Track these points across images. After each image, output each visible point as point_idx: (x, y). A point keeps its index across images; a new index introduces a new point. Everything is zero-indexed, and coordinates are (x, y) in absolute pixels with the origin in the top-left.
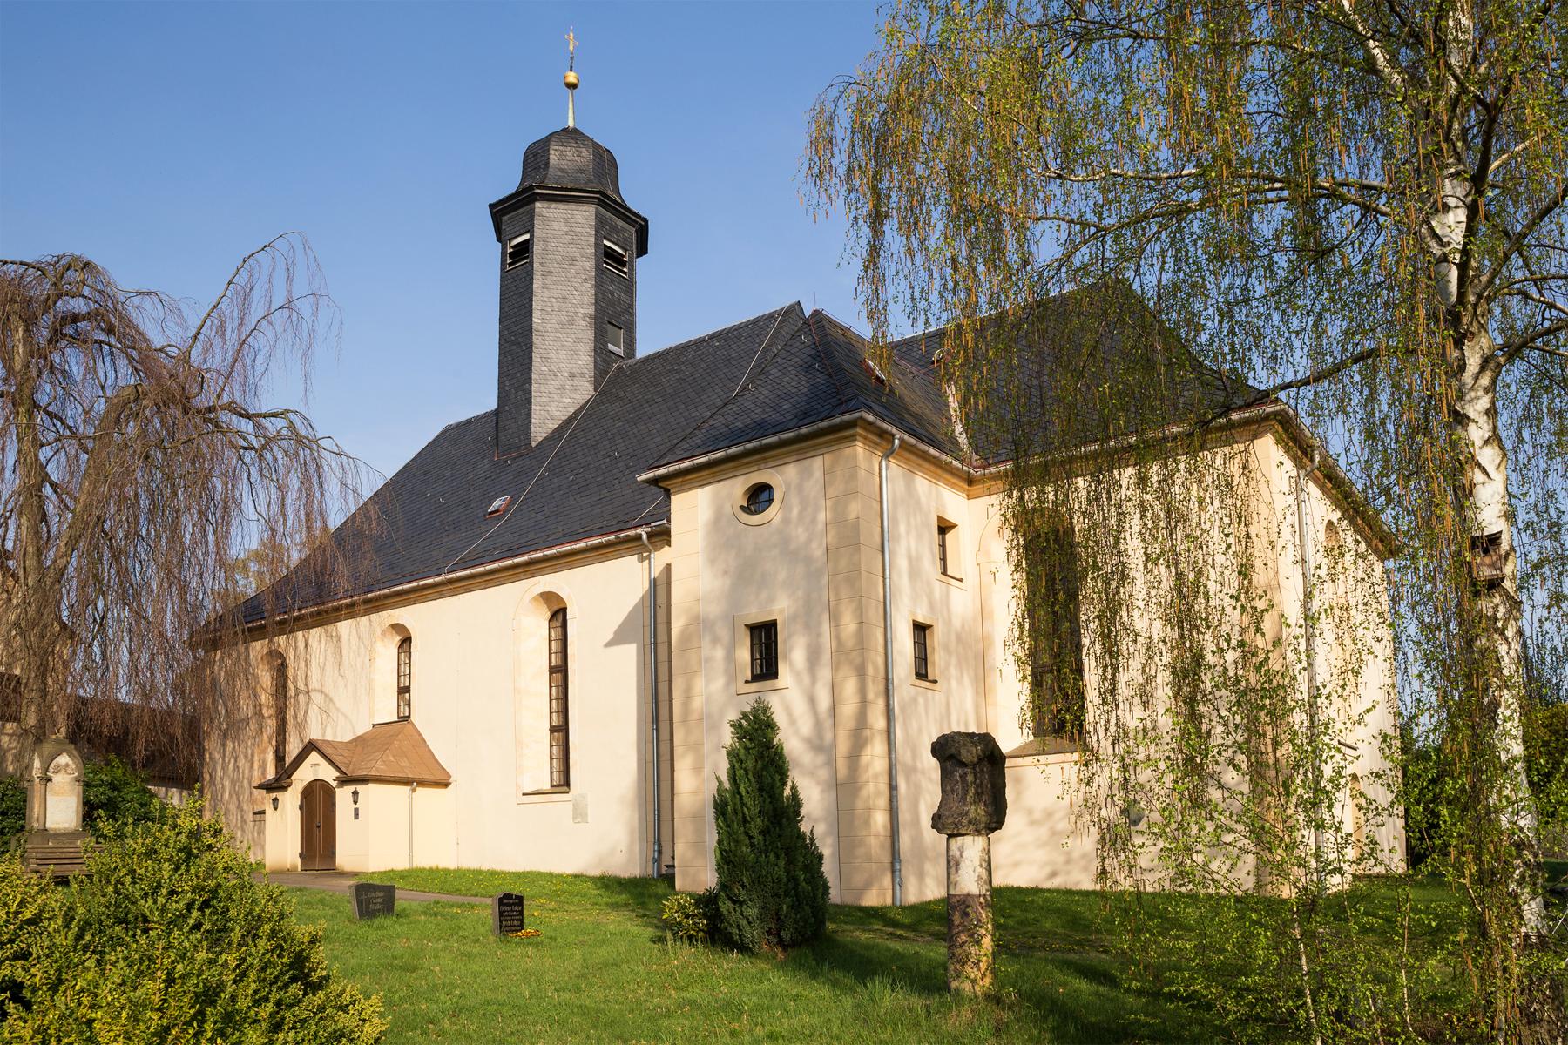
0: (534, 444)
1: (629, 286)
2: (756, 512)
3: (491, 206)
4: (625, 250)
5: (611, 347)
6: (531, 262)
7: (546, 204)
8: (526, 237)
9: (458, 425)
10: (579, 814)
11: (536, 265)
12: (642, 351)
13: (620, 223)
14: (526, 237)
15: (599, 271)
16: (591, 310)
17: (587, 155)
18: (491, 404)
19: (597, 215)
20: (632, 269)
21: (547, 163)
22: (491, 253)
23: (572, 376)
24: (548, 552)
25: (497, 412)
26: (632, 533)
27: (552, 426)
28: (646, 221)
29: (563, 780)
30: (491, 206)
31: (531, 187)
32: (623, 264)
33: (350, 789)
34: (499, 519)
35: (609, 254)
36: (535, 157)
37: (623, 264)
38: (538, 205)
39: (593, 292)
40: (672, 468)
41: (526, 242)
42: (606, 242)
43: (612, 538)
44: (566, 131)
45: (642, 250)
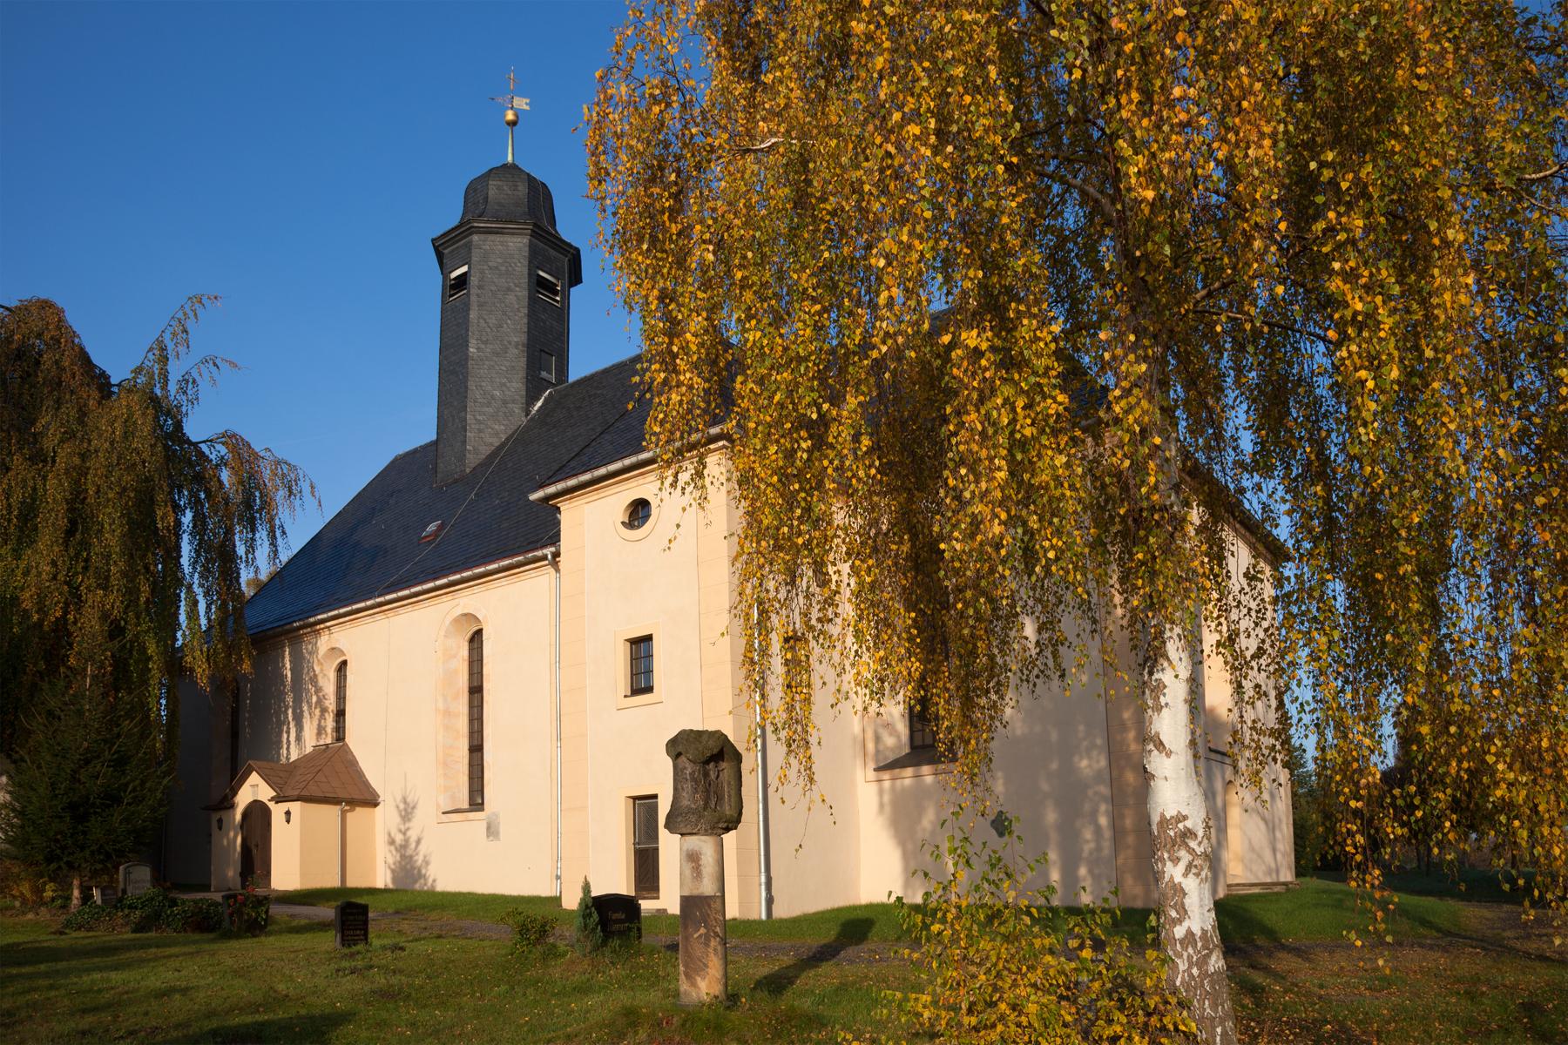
0: (468, 470)
1: (562, 315)
2: (639, 527)
3: (433, 241)
4: (558, 279)
5: (544, 374)
6: (468, 295)
7: (483, 237)
8: (464, 269)
9: (407, 454)
10: (492, 831)
11: (473, 298)
12: (576, 372)
13: (552, 252)
14: (464, 269)
15: (533, 301)
16: (523, 338)
17: (523, 189)
18: (434, 437)
19: (531, 245)
20: (566, 298)
21: (486, 198)
22: (432, 282)
23: (505, 402)
24: (465, 574)
25: (435, 444)
26: (539, 553)
27: (485, 451)
28: (578, 250)
29: (476, 800)
30: (433, 241)
31: (469, 222)
32: (556, 293)
33: (285, 806)
34: (430, 543)
35: (542, 283)
36: (475, 193)
37: (556, 293)
38: (475, 238)
39: (525, 320)
40: (560, 486)
41: (465, 274)
42: (542, 273)
43: (521, 558)
44: (505, 166)
45: (576, 278)
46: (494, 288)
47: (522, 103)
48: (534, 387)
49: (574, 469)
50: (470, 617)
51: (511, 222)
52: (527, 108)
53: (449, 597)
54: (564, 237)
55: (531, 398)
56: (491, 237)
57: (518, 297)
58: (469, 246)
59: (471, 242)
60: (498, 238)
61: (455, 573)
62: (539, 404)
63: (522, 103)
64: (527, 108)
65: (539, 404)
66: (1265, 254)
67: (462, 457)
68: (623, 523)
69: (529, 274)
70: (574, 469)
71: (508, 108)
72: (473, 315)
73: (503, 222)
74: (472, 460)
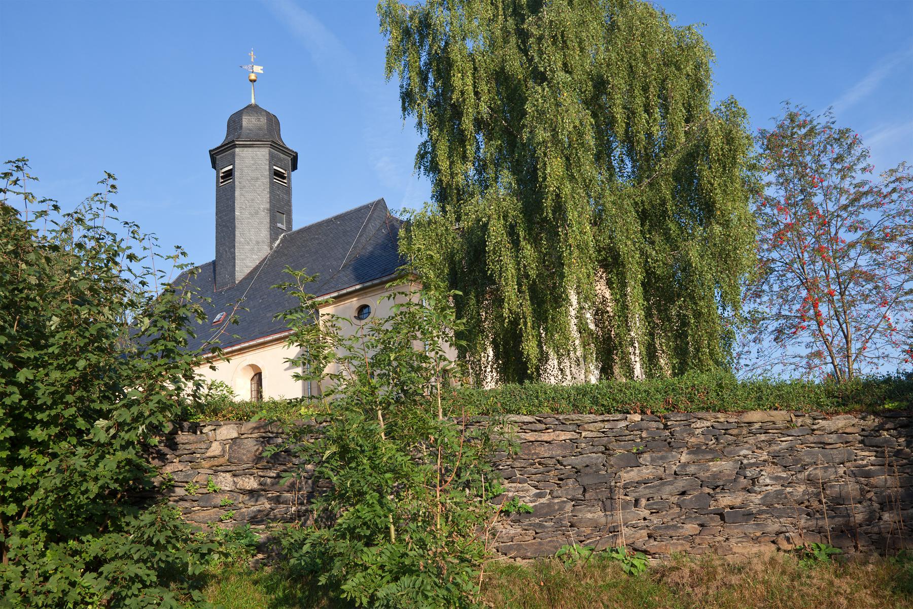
0: (237, 282)
1: (288, 191)
3: (210, 151)
5: (279, 225)
7: (241, 149)
8: (231, 167)
11: (237, 183)
13: (282, 156)
15: (272, 184)
16: (268, 206)
17: (263, 120)
19: (271, 155)
27: (247, 271)
28: (297, 154)
30: (210, 151)
31: (233, 141)
32: (284, 178)
36: (234, 123)
38: (237, 150)
42: (275, 167)
46: (249, 178)
47: (258, 69)
48: (274, 232)
49: (327, 290)
50: (253, 367)
51: (258, 141)
52: (262, 72)
53: (240, 356)
54: (288, 146)
55: (273, 239)
56: (246, 149)
57: (264, 181)
58: (233, 155)
59: (234, 153)
60: (250, 149)
61: (245, 342)
62: (278, 242)
63: (258, 69)
64: (262, 72)
65: (278, 242)
66: (530, 561)
67: (233, 274)
68: (355, 317)
69: (270, 169)
70: (327, 290)
71: (250, 72)
72: (237, 193)
73: (254, 141)
74: (240, 275)
